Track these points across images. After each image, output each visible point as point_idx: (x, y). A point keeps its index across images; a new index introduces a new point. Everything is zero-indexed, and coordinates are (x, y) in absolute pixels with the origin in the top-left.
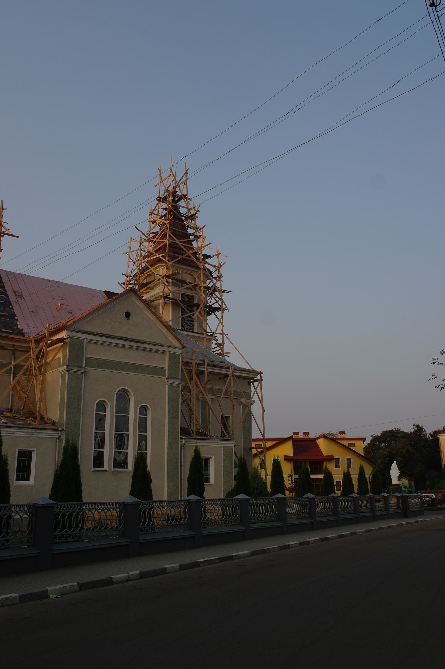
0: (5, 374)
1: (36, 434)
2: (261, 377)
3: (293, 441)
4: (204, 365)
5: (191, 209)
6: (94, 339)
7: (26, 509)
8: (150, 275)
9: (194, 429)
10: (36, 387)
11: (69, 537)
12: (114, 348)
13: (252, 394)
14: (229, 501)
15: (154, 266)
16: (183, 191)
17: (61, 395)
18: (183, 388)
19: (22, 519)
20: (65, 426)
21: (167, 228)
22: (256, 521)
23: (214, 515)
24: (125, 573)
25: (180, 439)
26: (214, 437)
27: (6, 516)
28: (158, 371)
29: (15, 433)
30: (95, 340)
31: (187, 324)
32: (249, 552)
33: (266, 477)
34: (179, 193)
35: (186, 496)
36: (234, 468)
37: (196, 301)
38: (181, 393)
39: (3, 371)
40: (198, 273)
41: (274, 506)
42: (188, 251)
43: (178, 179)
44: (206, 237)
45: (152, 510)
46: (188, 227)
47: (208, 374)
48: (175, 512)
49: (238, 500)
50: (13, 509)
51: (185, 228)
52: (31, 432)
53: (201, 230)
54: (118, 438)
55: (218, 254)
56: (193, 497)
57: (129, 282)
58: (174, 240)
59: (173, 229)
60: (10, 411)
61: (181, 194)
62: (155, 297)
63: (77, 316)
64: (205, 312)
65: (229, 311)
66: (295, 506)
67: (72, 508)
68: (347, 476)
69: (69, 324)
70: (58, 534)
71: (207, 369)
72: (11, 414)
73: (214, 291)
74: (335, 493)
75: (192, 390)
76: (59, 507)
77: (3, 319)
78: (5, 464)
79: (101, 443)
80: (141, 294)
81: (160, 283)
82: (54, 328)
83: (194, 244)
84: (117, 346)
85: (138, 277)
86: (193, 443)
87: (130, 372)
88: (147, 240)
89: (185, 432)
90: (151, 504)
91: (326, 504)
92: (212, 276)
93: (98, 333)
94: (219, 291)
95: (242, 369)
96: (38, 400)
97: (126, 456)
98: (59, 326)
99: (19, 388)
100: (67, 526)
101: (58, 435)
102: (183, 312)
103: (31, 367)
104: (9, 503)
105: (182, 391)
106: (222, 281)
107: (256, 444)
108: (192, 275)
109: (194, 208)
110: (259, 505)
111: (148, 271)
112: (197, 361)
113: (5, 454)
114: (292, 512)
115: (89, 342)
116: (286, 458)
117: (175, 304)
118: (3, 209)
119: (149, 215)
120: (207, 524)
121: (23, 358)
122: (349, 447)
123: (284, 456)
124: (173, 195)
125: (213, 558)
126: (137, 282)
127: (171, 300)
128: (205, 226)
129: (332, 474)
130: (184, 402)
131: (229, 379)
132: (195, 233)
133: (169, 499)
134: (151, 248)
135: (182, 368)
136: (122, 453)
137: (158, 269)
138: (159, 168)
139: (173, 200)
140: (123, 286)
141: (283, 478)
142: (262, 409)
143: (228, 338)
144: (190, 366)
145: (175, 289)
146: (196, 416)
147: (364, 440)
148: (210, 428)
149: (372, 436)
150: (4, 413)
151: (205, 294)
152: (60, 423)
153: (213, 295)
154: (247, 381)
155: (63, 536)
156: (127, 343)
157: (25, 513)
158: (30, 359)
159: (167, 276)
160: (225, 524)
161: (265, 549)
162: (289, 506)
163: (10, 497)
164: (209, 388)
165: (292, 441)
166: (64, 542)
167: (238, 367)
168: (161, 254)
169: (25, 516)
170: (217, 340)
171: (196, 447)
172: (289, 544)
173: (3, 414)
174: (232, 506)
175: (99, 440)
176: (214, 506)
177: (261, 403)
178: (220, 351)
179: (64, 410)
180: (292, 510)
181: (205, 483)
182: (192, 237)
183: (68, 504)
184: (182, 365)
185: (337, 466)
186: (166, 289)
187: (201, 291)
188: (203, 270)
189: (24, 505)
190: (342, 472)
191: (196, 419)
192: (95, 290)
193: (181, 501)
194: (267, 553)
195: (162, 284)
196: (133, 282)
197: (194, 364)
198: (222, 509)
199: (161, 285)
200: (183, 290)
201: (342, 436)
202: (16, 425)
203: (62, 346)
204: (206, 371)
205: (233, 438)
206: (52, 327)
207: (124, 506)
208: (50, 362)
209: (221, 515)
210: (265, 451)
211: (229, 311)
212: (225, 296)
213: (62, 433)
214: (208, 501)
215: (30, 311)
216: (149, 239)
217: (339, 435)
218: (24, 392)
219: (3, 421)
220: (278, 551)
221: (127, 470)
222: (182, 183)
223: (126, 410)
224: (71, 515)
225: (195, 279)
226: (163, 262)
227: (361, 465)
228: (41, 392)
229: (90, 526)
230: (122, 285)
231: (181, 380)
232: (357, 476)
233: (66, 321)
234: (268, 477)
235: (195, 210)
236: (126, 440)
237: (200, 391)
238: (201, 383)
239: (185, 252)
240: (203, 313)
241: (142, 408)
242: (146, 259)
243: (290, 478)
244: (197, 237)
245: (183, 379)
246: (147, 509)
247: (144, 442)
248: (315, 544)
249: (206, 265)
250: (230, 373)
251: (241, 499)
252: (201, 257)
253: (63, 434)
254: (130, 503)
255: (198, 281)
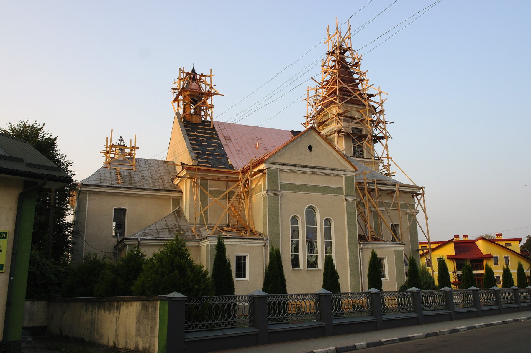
0: (222, 199)
1: (248, 243)
2: (423, 191)
3: (454, 243)
4: (374, 183)
5: (356, 58)
6: (285, 168)
7: (246, 298)
8: (325, 115)
9: (370, 236)
10: (245, 208)
11: (280, 320)
12: (302, 174)
13: (416, 205)
14: (403, 293)
15: (328, 108)
16: (347, 44)
17: (263, 213)
18: (358, 203)
19: (244, 307)
20: (268, 237)
21: (337, 76)
22: (427, 309)
23: (391, 304)
24: (324, 348)
25: (358, 244)
26: (386, 241)
27: (272, 302)
28: (337, 191)
29: (232, 242)
30: (287, 169)
31: (358, 152)
32: (423, 334)
33: (432, 273)
34: (344, 47)
35: (367, 289)
36: (405, 266)
37: (364, 133)
38: (357, 207)
39: (221, 197)
40: (364, 109)
41: (442, 297)
42: (355, 92)
43: (343, 36)
44: (369, 80)
45: (341, 300)
46: (354, 73)
47: (378, 191)
48: (363, 301)
49: (411, 292)
50: (237, 299)
51: (351, 74)
52: (244, 242)
53: (365, 74)
54: (309, 244)
55: (380, 93)
56: (373, 290)
57: (309, 122)
58: (343, 85)
59: (342, 76)
60: (228, 226)
61: (346, 47)
62: (330, 132)
63: (271, 152)
64: (372, 141)
65: (392, 138)
66: (461, 297)
67: (280, 298)
68: (507, 272)
69: (266, 158)
70: (271, 318)
71: (377, 187)
72: (229, 229)
73: (379, 123)
74: (496, 286)
75: (365, 204)
76: (270, 297)
77: (218, 158)
78: (229, 265)
79: (296, 248)
80: (319, 131)
81: (334, 120)
82: (255, 162)
83: (360, 86)
84: (303, 173)
85: (316, 117)
86: (369, 248)
87: (315, 192)
88: (321, 87)
89: (362, 238)
90: (340, 295)
91: (489, 295)
92: (376, 111)
93: (288, 164)
94: (383, 123)
95: (407, 186)
96: (247, 217)
97: (316, 258)
98: (258, 160)
99: (233, 209)
100: (277, 312)
101: (264, 243)
102: (354, 142)
103: (241, 192)
104: (234, 294)
105: (357, 205)
106: (385, 114)
107: (422, 247)
108: (359, 112)
109: (357, 57)
110: (429, 296)
111: (323, 112)
112: (368, 181)
113: (228, 258)
114: (458, 302)
115: (282, 171)
116: (450, 258)
117: (347, 136)
118: (212, 75)
119: (322, 67)
120: (386, 311)
121: (234, 186)
122: (506, 247)
123: (447, 255)
124: (339, 49)
125: (394, 338)
126: (315, 121)
127: (343, 134)
128: (367, 71)
129: (493, 270)
130: (359, 215)
131: (395, 194)
132: (359, 77)
133: (353, 292)
134: (325, 93)
135: (356, 187)
136: (313, 256)
137: (331, 109)
138: (327, 28)
139: (340, 53)
140: (305, 125)
141: (448, 274)
142: (426, 217)
143: (393, 161)
144: (363, 186)
145: (346, 124)
146: (370, 225)
147: (520, 240)
148: (382, 235)
149: (527, 237)
150: (224, 228)
151: (371, 126)
152: (265, 234)
153: (378, 126)
154: (411, 195)
155: (274, 319)
156: (311, 170)
157: (246, 302)
158: (239, 187)
159: (339, 115)
160: (401, 311)
161: (437, 332)
162: (455, 297)
163: (235, 290)
164: (379, 202)
165: (453, 243)
166: (276, 324)
167: (403, 184)
168: (333, 97)
169: (246, 304)
170: (384, 163)
171: (373, 250)
172: (458, 328)
173: (223, 229)
174: (406, 296)
175: (295, 246)
176: (296, 301)
177: (424, 212)
178: (386, 172)
179: (267, 224)
180: (458, 300)
181: (382, 279)
182: (357, 81)
183: (276, 295)
184: (356, 185)
185: (496, 263)
186: (339, 125)
187: (367, 124)
188: (368, 107)
189: (245, 296)
190: (502, 268)
191: (370, 228)
192: (283, 131)
193: (362, 293)
194: (439, 335)
195: (336, 121)
196: (312, 122)
197: (365, 183)
198: (398, 299)
199: (335, 122)
200: (353, 125)
201: (499, 238)
202: (233, 237)
203: (262, 175)
204: (376, 189)
205: (403, 242)
206: (253, 161)
207: (319, 297)
208: (254, 188)
209: (397, 304)
210: (430, 252)
211: (392, 138)
212: (388, 127)
213: (267, 242)
214: (386, 293)
215: (236, 151)
216: (323, 87)
217: (496, 237)
218: (237, 212)
219: (223, 234)
220: (449, 334)
221: (318, 269)
222: (347, 38)
223: (314, 223)
224: (279, 303)
225: (362, 115)
226: (335, 103)
227: (519, 262)
228: (249, 211)
229: (294, 312)
230: (304, 125)
231: (356, 197)
232: (517, 271)
233: (263, 156)
234: (434, 273)
235: (359, 59)
236: (315, 246)
237: (373, 205)
238: (372, 199)
239: (352, 93)
240: (370, 142)
241: (327, 220)
242: (322, 103)
243: (454, 274)
244: (361, 81)
245: (358, 196)
246: (337, 299)
247: (329, 247)
248: (481, 329)
249: (370, 103)
250: (396, 188)
251: (413, 291)
252: (366, 96)
253: (267, 242)
254: (323, 295)
255: (365, 116)
